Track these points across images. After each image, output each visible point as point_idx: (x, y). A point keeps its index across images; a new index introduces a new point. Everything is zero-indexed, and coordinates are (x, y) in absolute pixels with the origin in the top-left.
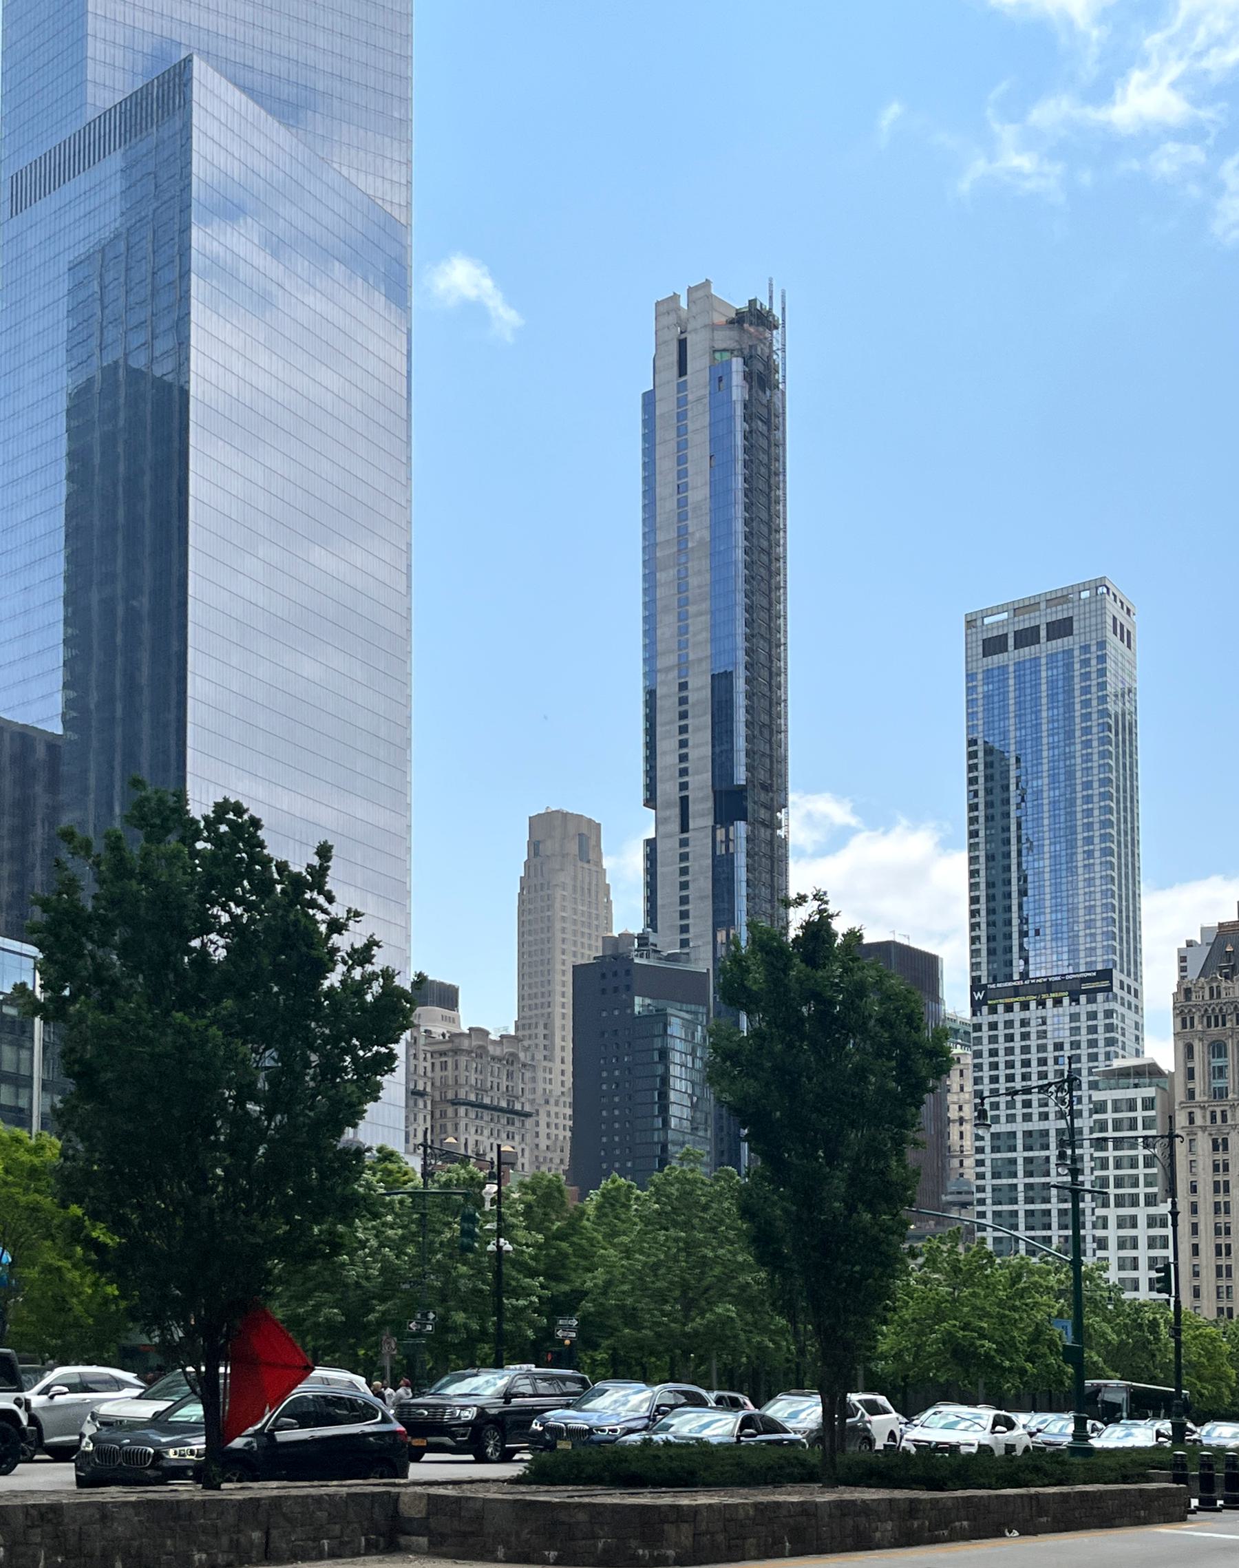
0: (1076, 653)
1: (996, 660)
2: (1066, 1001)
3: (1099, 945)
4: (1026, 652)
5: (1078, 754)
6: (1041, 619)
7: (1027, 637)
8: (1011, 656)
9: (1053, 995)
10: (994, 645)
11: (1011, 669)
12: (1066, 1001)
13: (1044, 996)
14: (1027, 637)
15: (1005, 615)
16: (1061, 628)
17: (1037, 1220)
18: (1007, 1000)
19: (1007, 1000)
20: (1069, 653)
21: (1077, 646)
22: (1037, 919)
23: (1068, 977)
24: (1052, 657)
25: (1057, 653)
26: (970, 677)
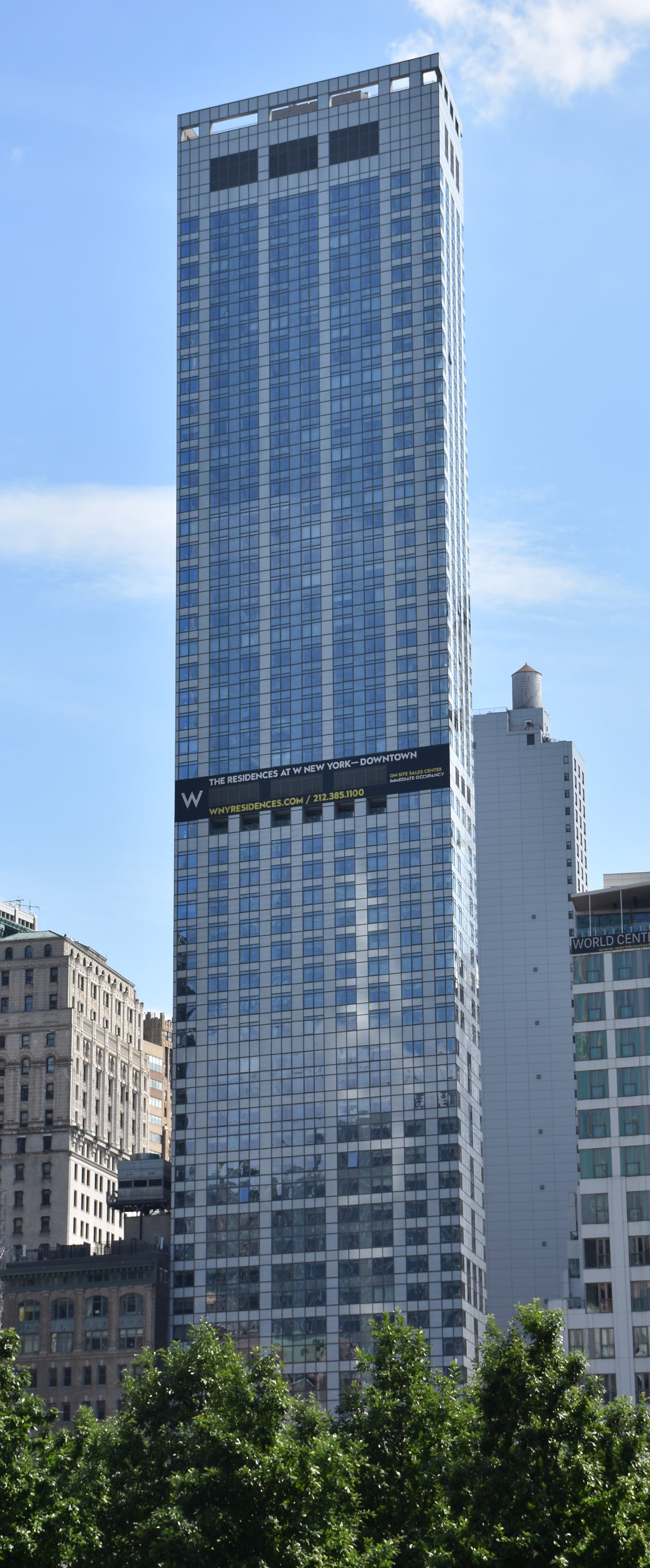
0: (385, 184)
1: (236, 196)
2: (360, 806)
3: (329, 908)
4: (293, 183)
5: (386, 361)
6: (321, 129)
7: (294, 157)
8: (263, 191)
9: (335, 796)
10: (231, 170)
11: (264, 211)
12: (360, 806)
13: (317, 798)
14: (294, 157)
15: (251, 120)
16: (357, 142)
17: (362, 1228)
18: (246, 808)
19: (246, 808)
20: (370, 184)
21: (385, 173)
22: (366, 353)
23: (363, 762)
24: (339, 192)
25: (348, 185)
26: (187, 224)
